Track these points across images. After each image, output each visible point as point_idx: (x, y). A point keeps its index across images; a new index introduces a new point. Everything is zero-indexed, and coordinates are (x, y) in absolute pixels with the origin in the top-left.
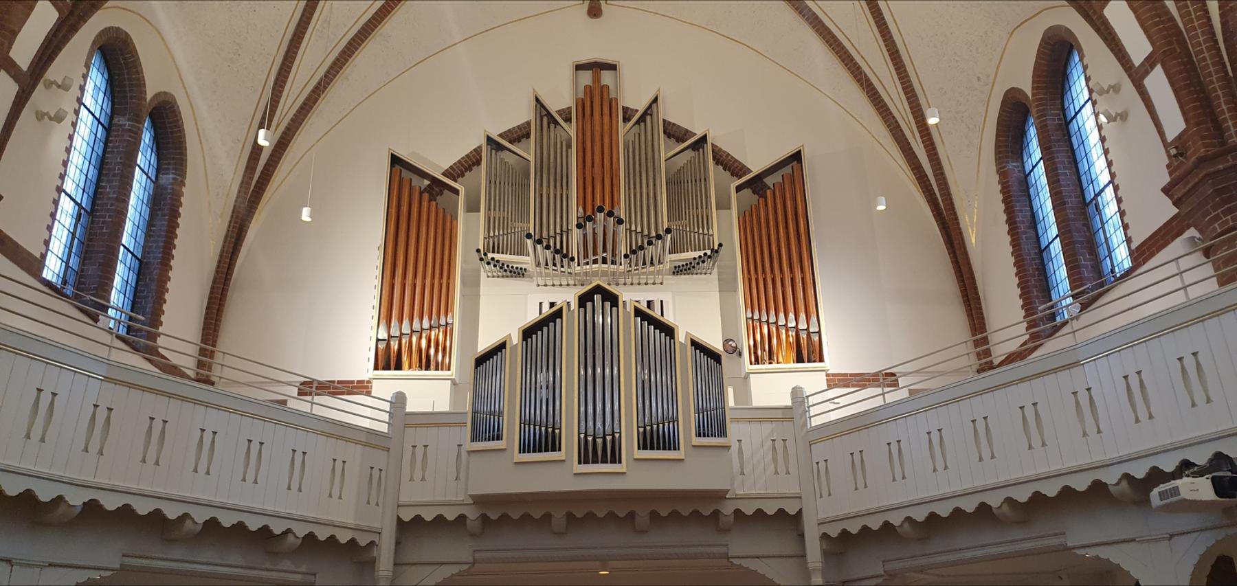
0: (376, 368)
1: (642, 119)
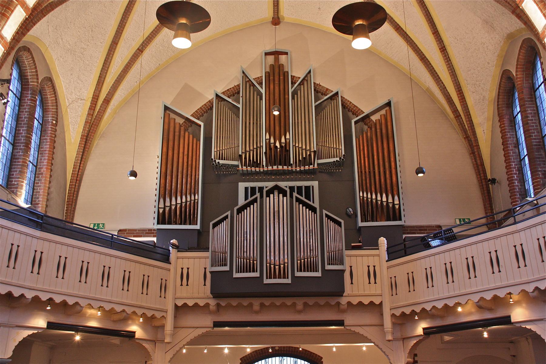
0: (158, 223)
1: (302, 83)
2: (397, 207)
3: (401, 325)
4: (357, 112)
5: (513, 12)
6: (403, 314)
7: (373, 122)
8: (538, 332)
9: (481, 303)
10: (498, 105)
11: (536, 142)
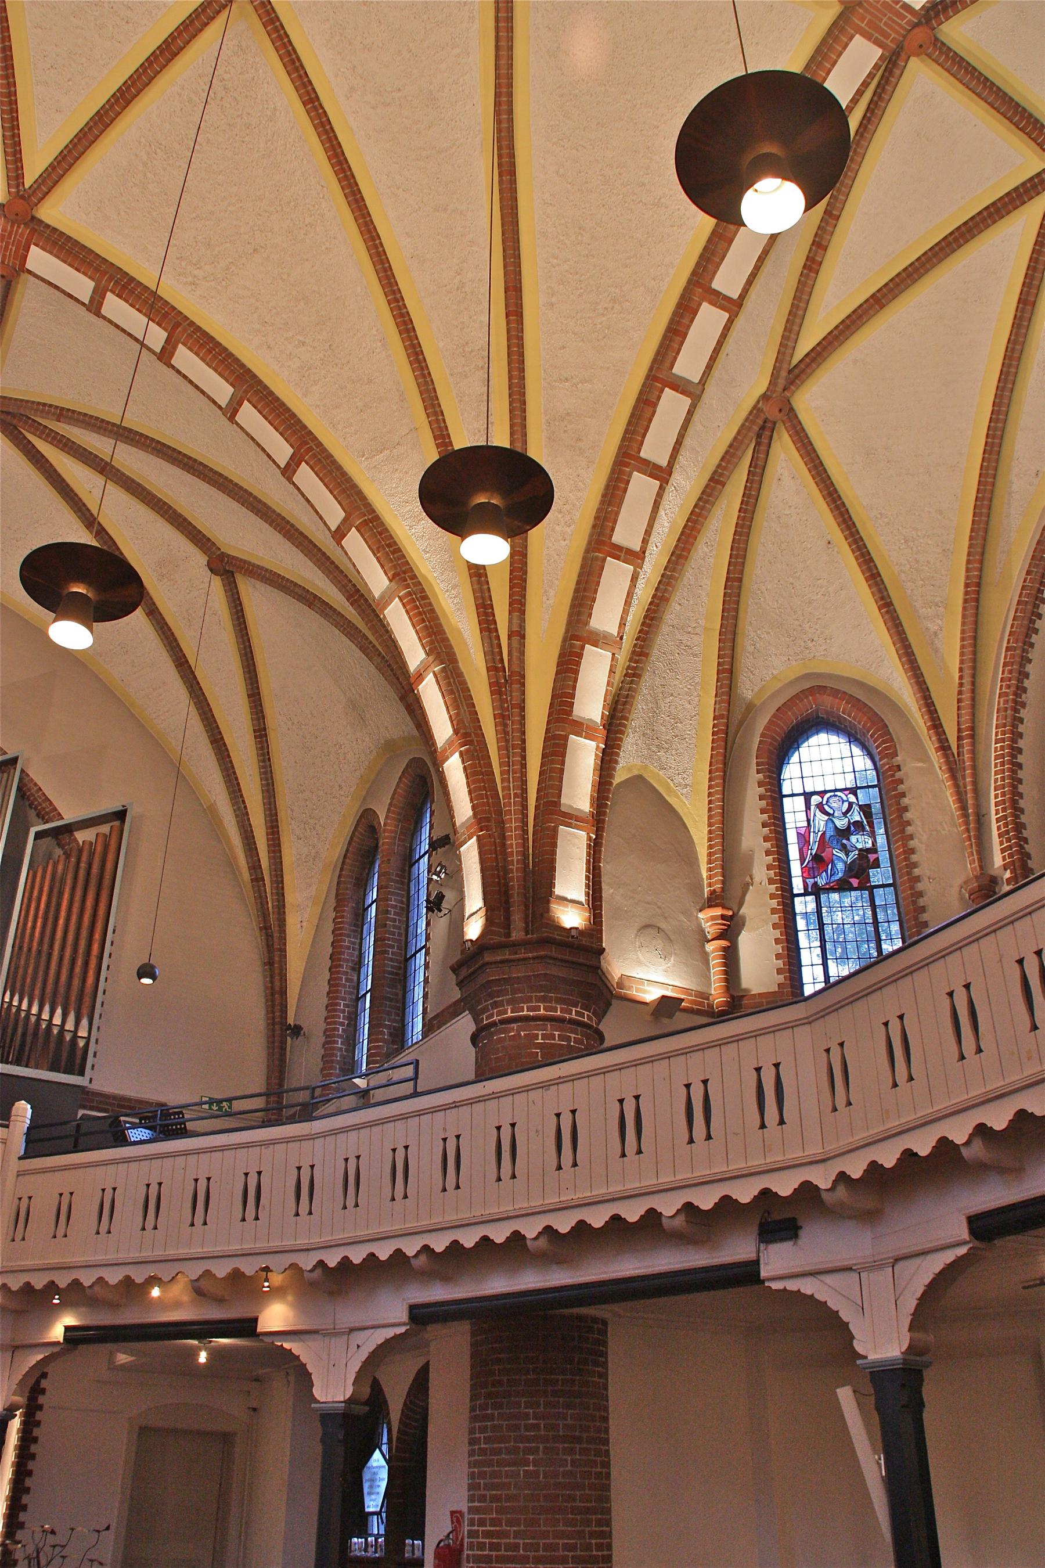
2: (81, 1043)
3: (18, 1313)
4: (47, 813)
5: (402, 698)
6: (28, 1287)
7: (78, 844)
8: (303, 1359)
9: (203, 1284)
10: (340, 876)
11: (392, 966)
